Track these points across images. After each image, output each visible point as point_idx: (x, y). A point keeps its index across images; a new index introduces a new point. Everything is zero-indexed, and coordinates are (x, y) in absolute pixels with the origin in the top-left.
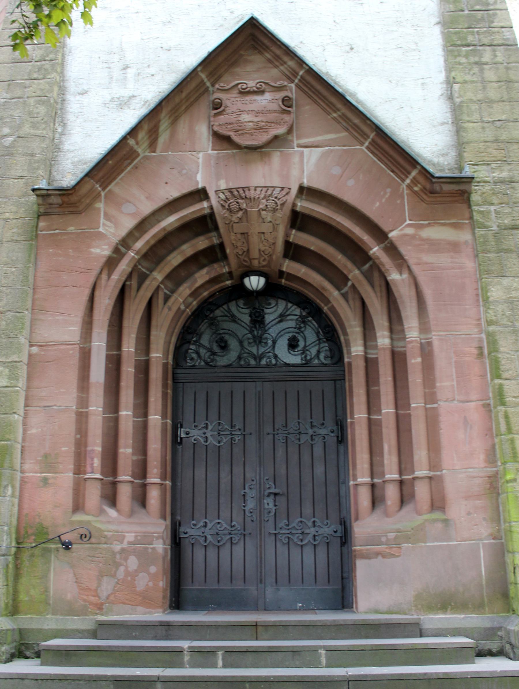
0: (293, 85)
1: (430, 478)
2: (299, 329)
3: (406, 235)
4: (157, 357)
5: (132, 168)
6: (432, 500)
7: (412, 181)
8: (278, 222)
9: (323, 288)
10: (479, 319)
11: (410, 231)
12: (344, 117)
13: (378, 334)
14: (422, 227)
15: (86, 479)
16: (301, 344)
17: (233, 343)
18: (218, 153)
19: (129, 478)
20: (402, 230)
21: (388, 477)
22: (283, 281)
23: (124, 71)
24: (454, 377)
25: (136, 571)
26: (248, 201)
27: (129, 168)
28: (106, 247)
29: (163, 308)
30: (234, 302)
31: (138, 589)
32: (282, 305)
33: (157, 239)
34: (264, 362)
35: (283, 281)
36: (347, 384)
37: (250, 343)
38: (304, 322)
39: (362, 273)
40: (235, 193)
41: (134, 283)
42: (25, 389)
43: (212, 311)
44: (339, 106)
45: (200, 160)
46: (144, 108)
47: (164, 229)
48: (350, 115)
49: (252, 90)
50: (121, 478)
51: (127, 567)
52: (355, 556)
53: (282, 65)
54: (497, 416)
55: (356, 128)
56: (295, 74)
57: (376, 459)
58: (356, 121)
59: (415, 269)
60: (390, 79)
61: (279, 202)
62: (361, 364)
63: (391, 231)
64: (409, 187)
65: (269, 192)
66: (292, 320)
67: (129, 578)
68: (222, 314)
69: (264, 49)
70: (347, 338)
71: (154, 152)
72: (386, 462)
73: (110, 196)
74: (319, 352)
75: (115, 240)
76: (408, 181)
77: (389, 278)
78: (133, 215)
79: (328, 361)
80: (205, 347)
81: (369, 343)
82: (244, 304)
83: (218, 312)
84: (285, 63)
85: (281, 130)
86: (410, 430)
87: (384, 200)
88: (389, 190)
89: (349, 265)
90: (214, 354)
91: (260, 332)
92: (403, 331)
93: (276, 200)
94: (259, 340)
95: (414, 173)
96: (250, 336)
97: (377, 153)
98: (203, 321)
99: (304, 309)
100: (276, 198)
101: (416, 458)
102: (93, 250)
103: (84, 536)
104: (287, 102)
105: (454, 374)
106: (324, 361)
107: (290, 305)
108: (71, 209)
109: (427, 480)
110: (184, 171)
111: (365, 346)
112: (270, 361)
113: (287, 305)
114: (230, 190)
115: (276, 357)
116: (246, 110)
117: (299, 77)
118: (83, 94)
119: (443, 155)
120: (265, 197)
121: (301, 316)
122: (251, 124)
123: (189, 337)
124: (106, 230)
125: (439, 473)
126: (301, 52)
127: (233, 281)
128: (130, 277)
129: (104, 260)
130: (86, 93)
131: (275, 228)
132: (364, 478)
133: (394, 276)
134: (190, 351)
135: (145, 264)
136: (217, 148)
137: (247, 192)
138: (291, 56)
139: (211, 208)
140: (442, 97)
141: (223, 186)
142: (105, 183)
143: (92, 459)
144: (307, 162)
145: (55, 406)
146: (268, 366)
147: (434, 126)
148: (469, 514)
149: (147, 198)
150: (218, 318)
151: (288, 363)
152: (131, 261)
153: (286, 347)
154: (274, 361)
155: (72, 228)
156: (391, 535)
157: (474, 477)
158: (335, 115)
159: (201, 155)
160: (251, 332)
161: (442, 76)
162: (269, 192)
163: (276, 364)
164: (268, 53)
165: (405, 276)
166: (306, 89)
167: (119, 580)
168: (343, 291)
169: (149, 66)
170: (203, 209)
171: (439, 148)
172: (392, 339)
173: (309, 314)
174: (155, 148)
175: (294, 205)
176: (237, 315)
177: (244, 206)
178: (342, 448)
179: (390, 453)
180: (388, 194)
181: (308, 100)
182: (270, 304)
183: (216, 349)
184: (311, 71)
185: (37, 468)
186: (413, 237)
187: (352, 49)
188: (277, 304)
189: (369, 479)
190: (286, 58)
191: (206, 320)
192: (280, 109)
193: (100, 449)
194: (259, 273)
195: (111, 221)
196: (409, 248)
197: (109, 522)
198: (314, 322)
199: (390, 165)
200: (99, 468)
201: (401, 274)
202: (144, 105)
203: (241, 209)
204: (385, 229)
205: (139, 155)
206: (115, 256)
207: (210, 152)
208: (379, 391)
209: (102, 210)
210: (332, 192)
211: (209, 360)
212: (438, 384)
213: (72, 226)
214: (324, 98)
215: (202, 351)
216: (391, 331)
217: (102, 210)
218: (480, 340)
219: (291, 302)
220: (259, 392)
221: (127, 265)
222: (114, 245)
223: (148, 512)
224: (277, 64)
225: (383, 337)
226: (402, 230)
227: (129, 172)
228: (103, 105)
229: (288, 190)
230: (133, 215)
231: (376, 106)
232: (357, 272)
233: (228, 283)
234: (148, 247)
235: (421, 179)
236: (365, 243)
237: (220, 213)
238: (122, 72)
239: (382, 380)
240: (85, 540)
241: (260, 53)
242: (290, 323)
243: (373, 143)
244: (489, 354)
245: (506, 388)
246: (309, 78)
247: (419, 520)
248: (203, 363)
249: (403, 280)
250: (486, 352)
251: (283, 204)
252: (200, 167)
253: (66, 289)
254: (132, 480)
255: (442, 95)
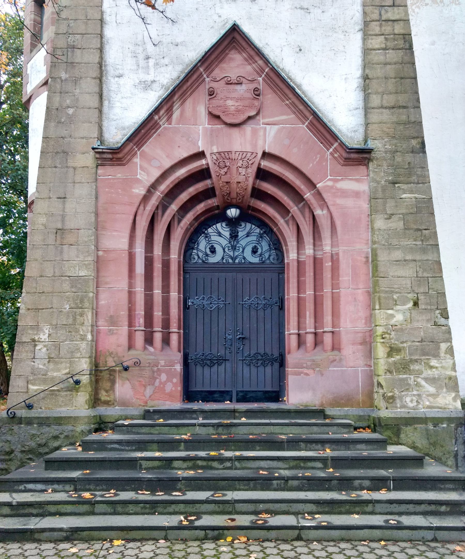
0: (260, 79)
1: (333, 332)
2: (259, 242)
3: (328, 186)
4: (175, 258)
5: (156, 135)
6: (333, 344)
7: (333, 150)
8: (249, 176)
9: (275, 217)
10: (368, 240)
11: (330, 183)
12: (293, 104)
13: (306, 247)
14: (338, 181)
15: (135, 330)
16: (259, 251)
17: (219, 250)
18: (212, 127)
19: (160, 329)
20: (324, 182)
21: (308, 330)
22: (250, 211)
23: (146, 61)
24: (350, 275)
25: (165, 382)
26: (231, 161)
27: (155, 135)
28: (142, 189)
29: (177, 228)
30: (220, 224)
31: (166, 392)
32: (249, 225)
33: (174, 184)
34: (237, 261)
35: (250, 211)
36: (286, 276)
37: (229, 249)
38: (261, 237)
39: (299, 209)
40: (223, 155)
41: (160, 212)
42: (96, 277)
43: (206, 229)
44: (291, 96)
45: (201, 131)
46: (162, 90)
47: (178, 178)
48: (297, 102)
49: (234, 82)
50: (155, 329)
51: (160, 379)
52: (287, 374)
53: (254, 63)
54: (374, 298)
55: (300, 112)
56: (263, 70)
57: (302, 320)
58: (301, 107)
59: (331, 208)
60: (324, 75)
61: (250, 162)
62: (295, 264)
63: (318, 183)
64: (331, 154)
65: (244, 155)
66: (255, 235)
67: (162, 386)
68: (213, 231)
69: (243, 50)
70: (287, 248)
71: (170, 124)
72: (307, 322)
73: (143, 156)
74: (270, 256)
75: (148, 184)
76: (331, 150)
77: (315, 213)
78: (159, 167)
79: (275, 262)
80: (202, 251)
81: (300, 252)
82: (226, 225)
83: (210, 230)
84: (256, 62)
85: (253, 113)
86: (322, 304)
87: (315, 163)
88: (319, 156)
89: (291, 204)
90: (207, 255)
91: (235, 243)
92: (321, 245)
93: (248, 161)
94: (234, 248)
95: (336, 145)
96: (229, 245)
97: (313, 130)
98: (201, 235)
99: (262, 230)
100: (248, 159)
101: (325, 321)
102: (134, 190)
103: (136, 363)
104: (257, 93)
105: (351, 273)
106: (272, 262)
107: (253, 226)
108: (119, 163)
109: (331, 334)
110: (190, 139)
111: (298, 253)
112: (241, 261)
113: (251, 227)
114: (219, 153)
115: (244, 258)
116: (230, 97)
117: (265, 73)
118: (119, 77)
119: (355, 131)
120: (241, 159)
121: (260, 234)
122: (233, 107)
123: (192, 245)
124: (142, 177)
125: (338, 329)
126: (267, 51)
127: (220, 211)
128: (157, 208)
129: (141, 197)
130: (122, 76)
131: (247, 179)
132: (294, 330)
133: (318, 212)
134: (193, 253)
135: (167, 199)
136: (211, 123)
137: (230, 155)
138: (260, 57)
139: (208, 164)
140: (357, 89)
141: (215, 150)
142: (140, 144)
143: (139, 319)
144: (269, 135)
145: (115, 287)
146: (239, 263)
147: (350, 111)
148: (354, 353)
149: (167, 156)
150: (210, 234)
151: (251, 262)
152: (158, 198)
153: (250, 252)
154: (243, 261)
155: (120, 175)
156: (309, 363)
157: (358, 332)
158: (287, 102)
159: (201, 127)
160: (230, 242)
161: (359, 73)
162: (244, 155)
163: (244, 263)
164: (245, 53)
165: (325, 212)
166: (269, 82)
167: (156, 387)
168: (286, 219)
169: (163, 58)
170: (203, 165)
171: (352, 126)
172: (314, 250)
173: (265, 232)
174: (171, 122)
175: (259, 164)
176: (222, 233)
177: (228, 164)
178: (281, 311)
179: (310, 317)
180: (318, 158)
181: (270, 91)
182: (241, 225)
183: (208, 252)
184: (273, 69)
185: (106, 324)
186: (332, 187)
187: (300, 50)
188: (246, 226)
189: (297, 331)
190: (257, 58)
191: (203, 235)
192: (252, 97)
193: (143, 313)
194: (236, 206)
195: (144, 172)
196: (329, 194)
197: (150, 355)
198: (267, 237)
199: (320, 138)
200: (143, 324)
201: (322, 210)
202: (162, 88)
203: (226, 166)
204: (315, 182)
205: (160, 126)
206: (148, 194)
207: (207, 126)
208: (305, 281)
209: (139, 163)
210: (283, 156)
211: (204, 259)
212: (340, 279)
213: (119, 173)
214: (281, 90)
215: (201, 254)
216: (314, 245)
217: (139, 163)
218: (367, 253)
219: (254, 225)
220: (234, 279)
221: (156, 201)
222: (147, 187)
223: (171, 349)
224: (251, 62)
225: (309, 249)
226: (324, 182)
227: (155, 138)
228: (134, 87)
229: (256, 154)
230: (159, 167)
231: (314, 95)
232: (296, 208)
233: (217, 212)
234: (168, 189)
235: (340, 149)
236: (302, 190)
237: (213, 169)
238: (145, 62)
239: (307, 275)
240: (137, 365)
241: (240, 53)
242: (253, 238)
243: (311, 123)
244: (372, 261)
245: (380, 282)
246: (272, 74)
247: (324, 355)
248: (200, 261)
249: (323, 214)
250: (370, 260)
251: (252, 164)
252: (201, 136)
253: (118, 215)
254: (162, 330)
255: (358, 87)
